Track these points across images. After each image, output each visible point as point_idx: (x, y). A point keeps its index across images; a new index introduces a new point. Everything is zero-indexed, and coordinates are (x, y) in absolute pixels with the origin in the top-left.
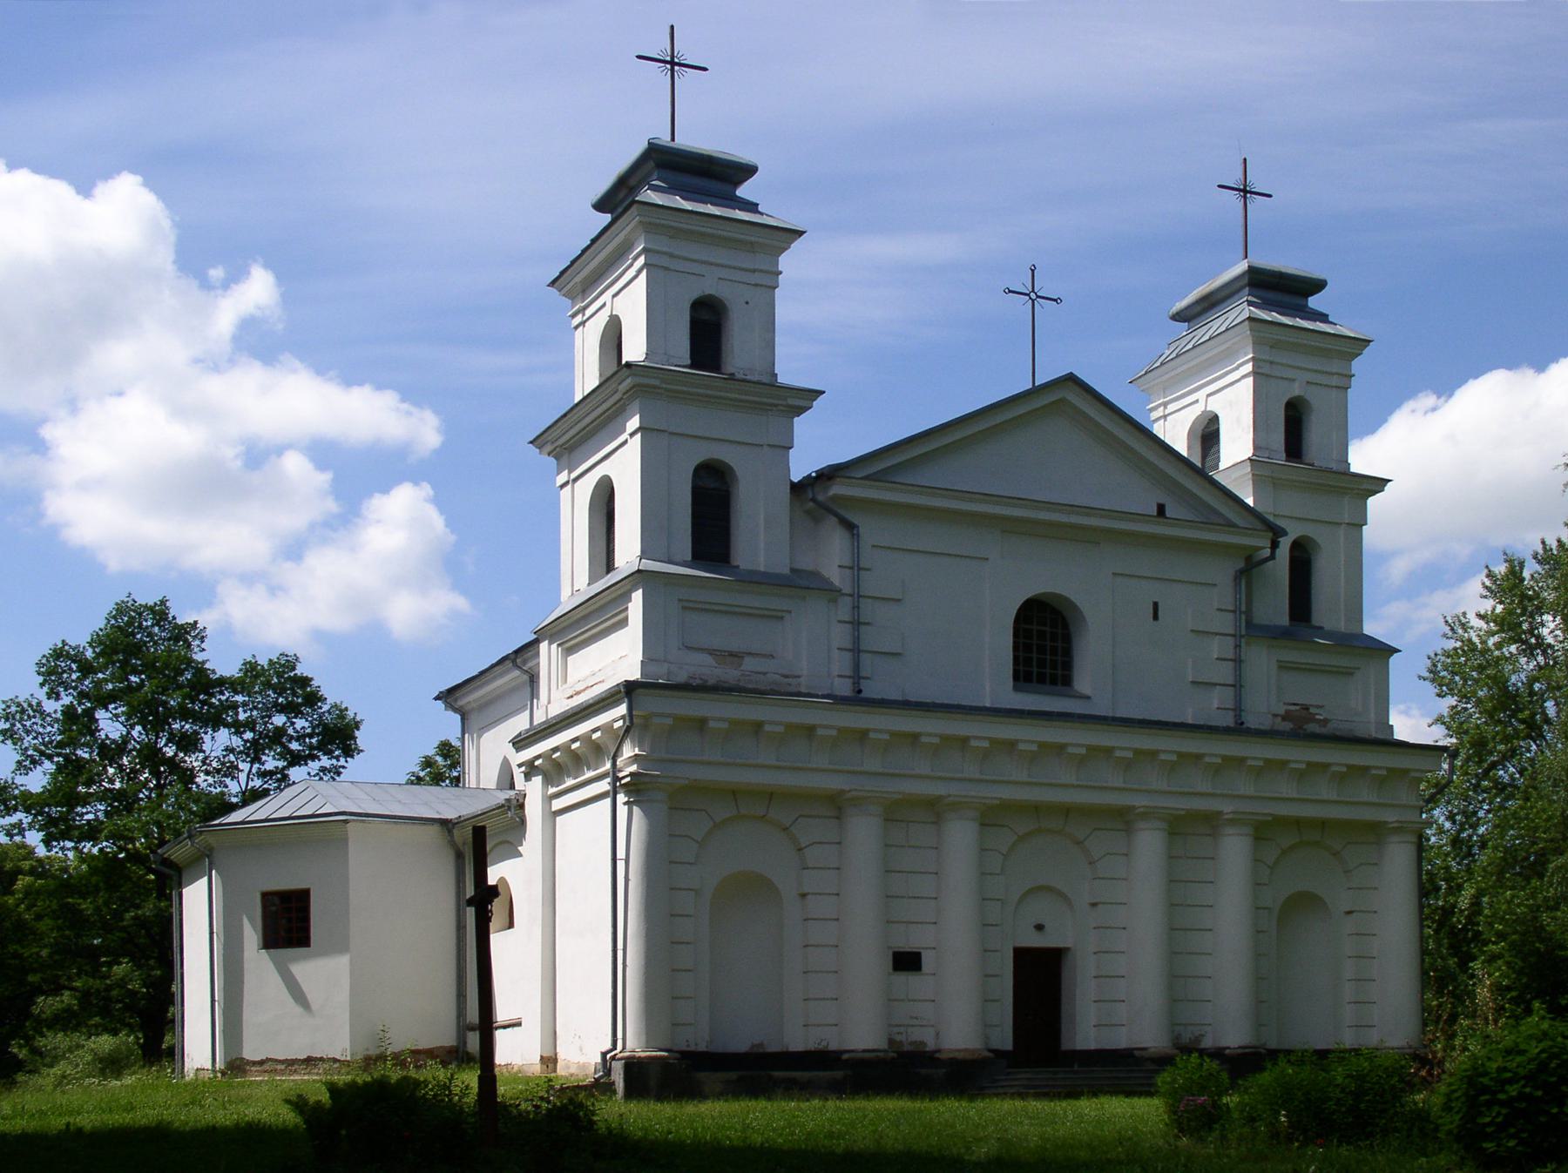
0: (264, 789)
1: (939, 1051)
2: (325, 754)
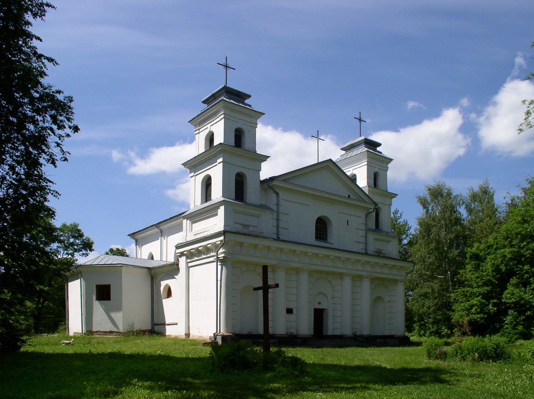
1: (298, 335)
2: (84, 250)
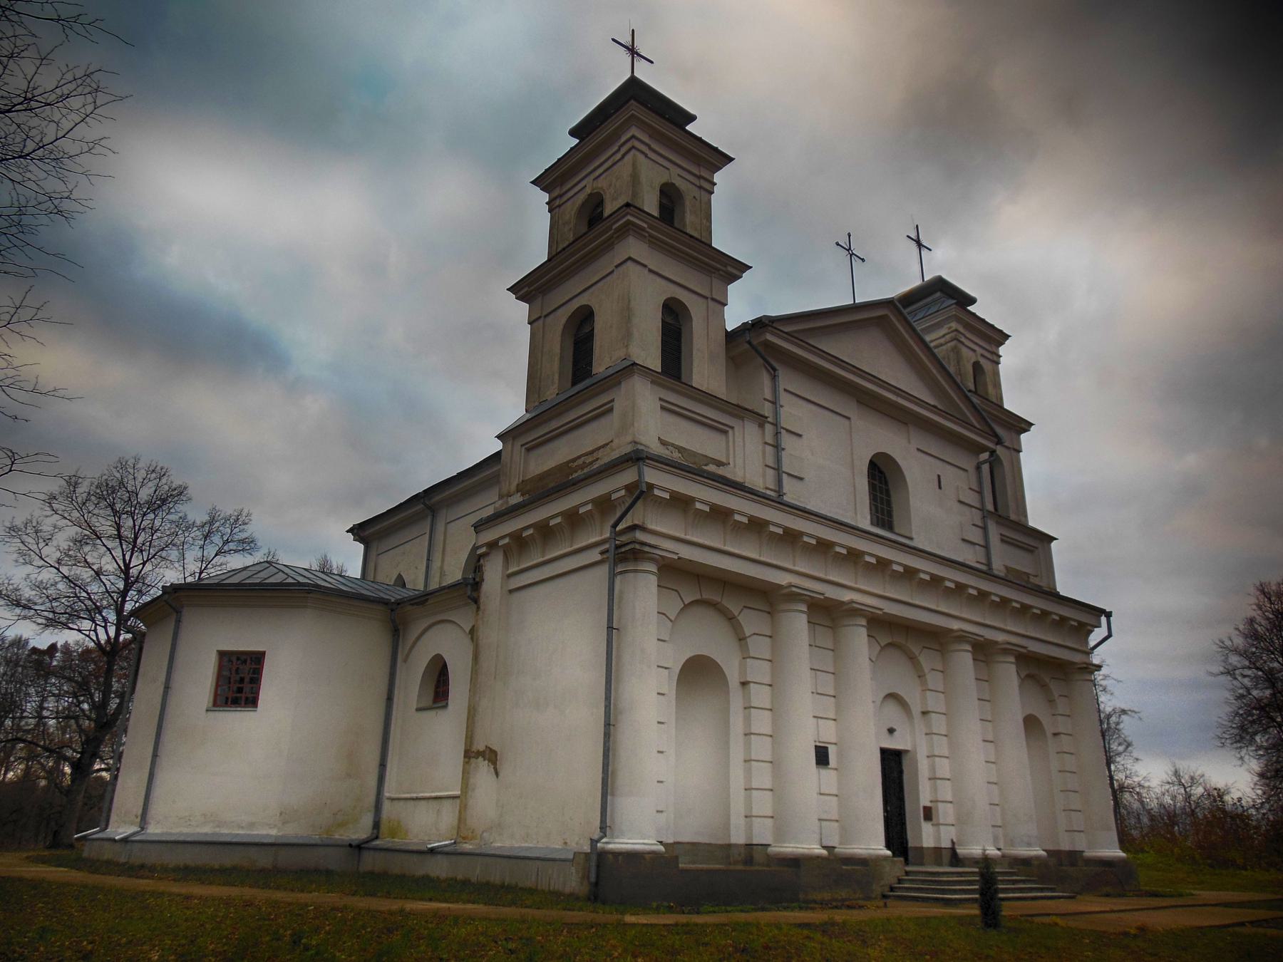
0: (101, 777)
